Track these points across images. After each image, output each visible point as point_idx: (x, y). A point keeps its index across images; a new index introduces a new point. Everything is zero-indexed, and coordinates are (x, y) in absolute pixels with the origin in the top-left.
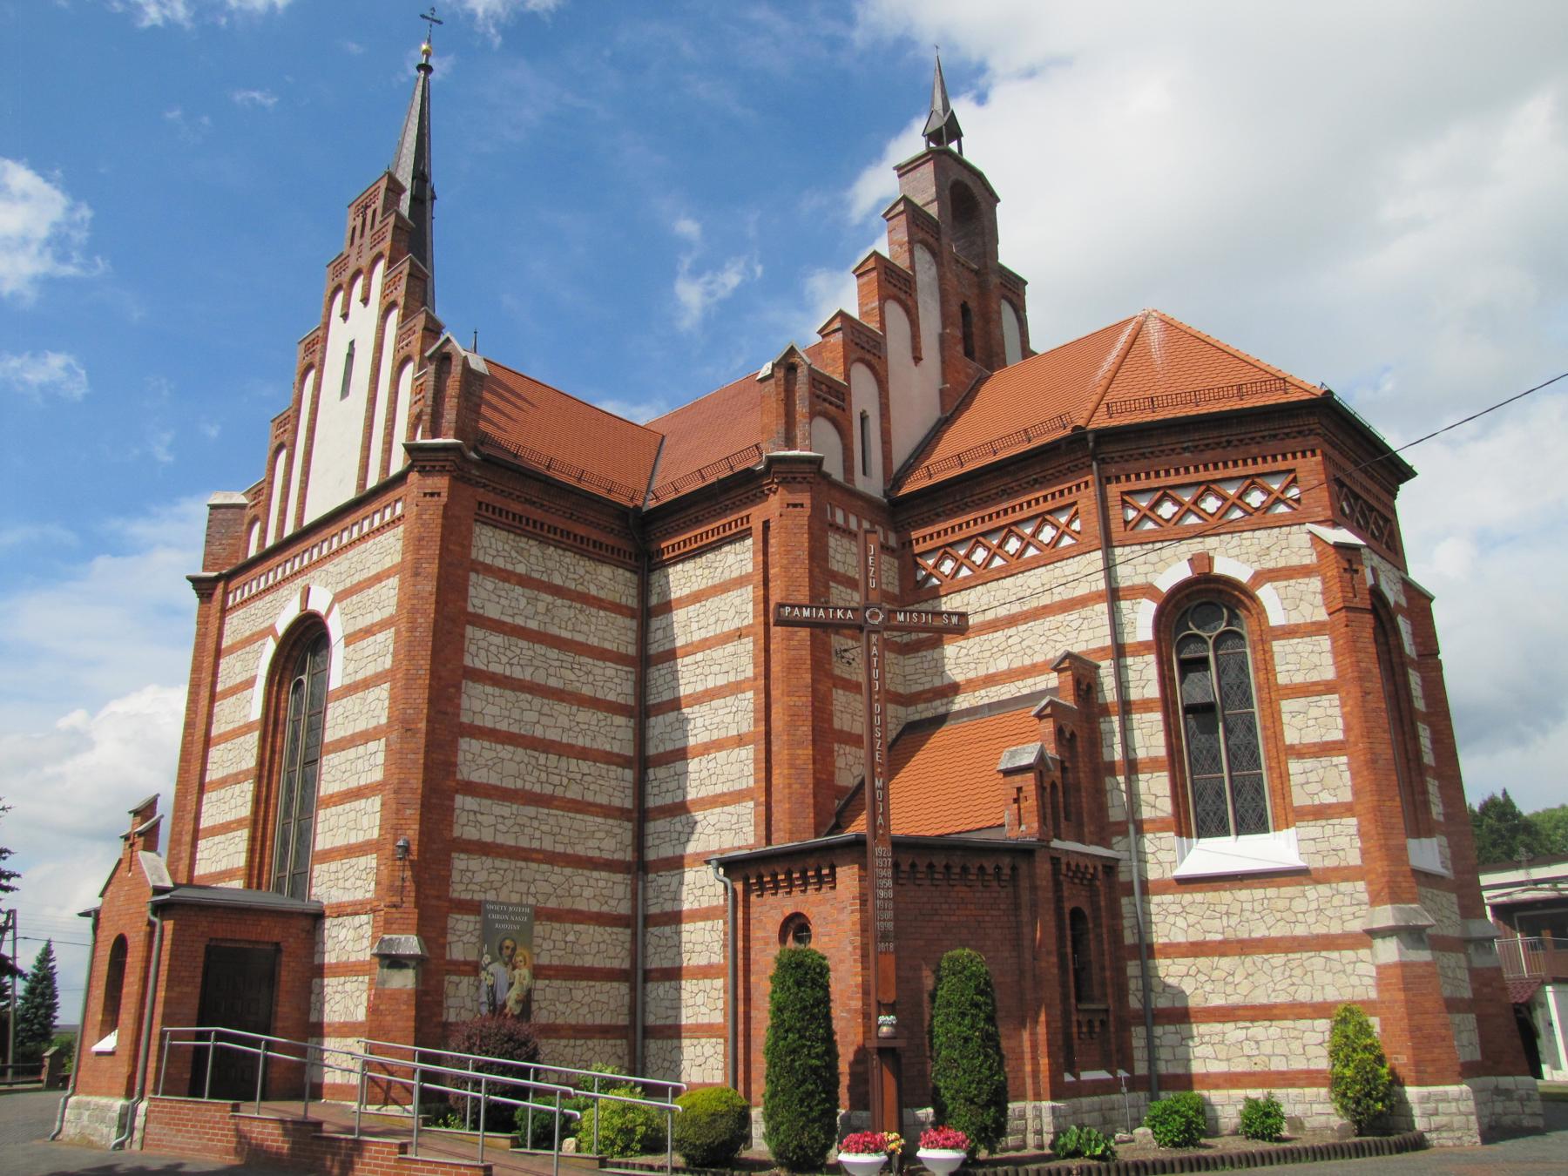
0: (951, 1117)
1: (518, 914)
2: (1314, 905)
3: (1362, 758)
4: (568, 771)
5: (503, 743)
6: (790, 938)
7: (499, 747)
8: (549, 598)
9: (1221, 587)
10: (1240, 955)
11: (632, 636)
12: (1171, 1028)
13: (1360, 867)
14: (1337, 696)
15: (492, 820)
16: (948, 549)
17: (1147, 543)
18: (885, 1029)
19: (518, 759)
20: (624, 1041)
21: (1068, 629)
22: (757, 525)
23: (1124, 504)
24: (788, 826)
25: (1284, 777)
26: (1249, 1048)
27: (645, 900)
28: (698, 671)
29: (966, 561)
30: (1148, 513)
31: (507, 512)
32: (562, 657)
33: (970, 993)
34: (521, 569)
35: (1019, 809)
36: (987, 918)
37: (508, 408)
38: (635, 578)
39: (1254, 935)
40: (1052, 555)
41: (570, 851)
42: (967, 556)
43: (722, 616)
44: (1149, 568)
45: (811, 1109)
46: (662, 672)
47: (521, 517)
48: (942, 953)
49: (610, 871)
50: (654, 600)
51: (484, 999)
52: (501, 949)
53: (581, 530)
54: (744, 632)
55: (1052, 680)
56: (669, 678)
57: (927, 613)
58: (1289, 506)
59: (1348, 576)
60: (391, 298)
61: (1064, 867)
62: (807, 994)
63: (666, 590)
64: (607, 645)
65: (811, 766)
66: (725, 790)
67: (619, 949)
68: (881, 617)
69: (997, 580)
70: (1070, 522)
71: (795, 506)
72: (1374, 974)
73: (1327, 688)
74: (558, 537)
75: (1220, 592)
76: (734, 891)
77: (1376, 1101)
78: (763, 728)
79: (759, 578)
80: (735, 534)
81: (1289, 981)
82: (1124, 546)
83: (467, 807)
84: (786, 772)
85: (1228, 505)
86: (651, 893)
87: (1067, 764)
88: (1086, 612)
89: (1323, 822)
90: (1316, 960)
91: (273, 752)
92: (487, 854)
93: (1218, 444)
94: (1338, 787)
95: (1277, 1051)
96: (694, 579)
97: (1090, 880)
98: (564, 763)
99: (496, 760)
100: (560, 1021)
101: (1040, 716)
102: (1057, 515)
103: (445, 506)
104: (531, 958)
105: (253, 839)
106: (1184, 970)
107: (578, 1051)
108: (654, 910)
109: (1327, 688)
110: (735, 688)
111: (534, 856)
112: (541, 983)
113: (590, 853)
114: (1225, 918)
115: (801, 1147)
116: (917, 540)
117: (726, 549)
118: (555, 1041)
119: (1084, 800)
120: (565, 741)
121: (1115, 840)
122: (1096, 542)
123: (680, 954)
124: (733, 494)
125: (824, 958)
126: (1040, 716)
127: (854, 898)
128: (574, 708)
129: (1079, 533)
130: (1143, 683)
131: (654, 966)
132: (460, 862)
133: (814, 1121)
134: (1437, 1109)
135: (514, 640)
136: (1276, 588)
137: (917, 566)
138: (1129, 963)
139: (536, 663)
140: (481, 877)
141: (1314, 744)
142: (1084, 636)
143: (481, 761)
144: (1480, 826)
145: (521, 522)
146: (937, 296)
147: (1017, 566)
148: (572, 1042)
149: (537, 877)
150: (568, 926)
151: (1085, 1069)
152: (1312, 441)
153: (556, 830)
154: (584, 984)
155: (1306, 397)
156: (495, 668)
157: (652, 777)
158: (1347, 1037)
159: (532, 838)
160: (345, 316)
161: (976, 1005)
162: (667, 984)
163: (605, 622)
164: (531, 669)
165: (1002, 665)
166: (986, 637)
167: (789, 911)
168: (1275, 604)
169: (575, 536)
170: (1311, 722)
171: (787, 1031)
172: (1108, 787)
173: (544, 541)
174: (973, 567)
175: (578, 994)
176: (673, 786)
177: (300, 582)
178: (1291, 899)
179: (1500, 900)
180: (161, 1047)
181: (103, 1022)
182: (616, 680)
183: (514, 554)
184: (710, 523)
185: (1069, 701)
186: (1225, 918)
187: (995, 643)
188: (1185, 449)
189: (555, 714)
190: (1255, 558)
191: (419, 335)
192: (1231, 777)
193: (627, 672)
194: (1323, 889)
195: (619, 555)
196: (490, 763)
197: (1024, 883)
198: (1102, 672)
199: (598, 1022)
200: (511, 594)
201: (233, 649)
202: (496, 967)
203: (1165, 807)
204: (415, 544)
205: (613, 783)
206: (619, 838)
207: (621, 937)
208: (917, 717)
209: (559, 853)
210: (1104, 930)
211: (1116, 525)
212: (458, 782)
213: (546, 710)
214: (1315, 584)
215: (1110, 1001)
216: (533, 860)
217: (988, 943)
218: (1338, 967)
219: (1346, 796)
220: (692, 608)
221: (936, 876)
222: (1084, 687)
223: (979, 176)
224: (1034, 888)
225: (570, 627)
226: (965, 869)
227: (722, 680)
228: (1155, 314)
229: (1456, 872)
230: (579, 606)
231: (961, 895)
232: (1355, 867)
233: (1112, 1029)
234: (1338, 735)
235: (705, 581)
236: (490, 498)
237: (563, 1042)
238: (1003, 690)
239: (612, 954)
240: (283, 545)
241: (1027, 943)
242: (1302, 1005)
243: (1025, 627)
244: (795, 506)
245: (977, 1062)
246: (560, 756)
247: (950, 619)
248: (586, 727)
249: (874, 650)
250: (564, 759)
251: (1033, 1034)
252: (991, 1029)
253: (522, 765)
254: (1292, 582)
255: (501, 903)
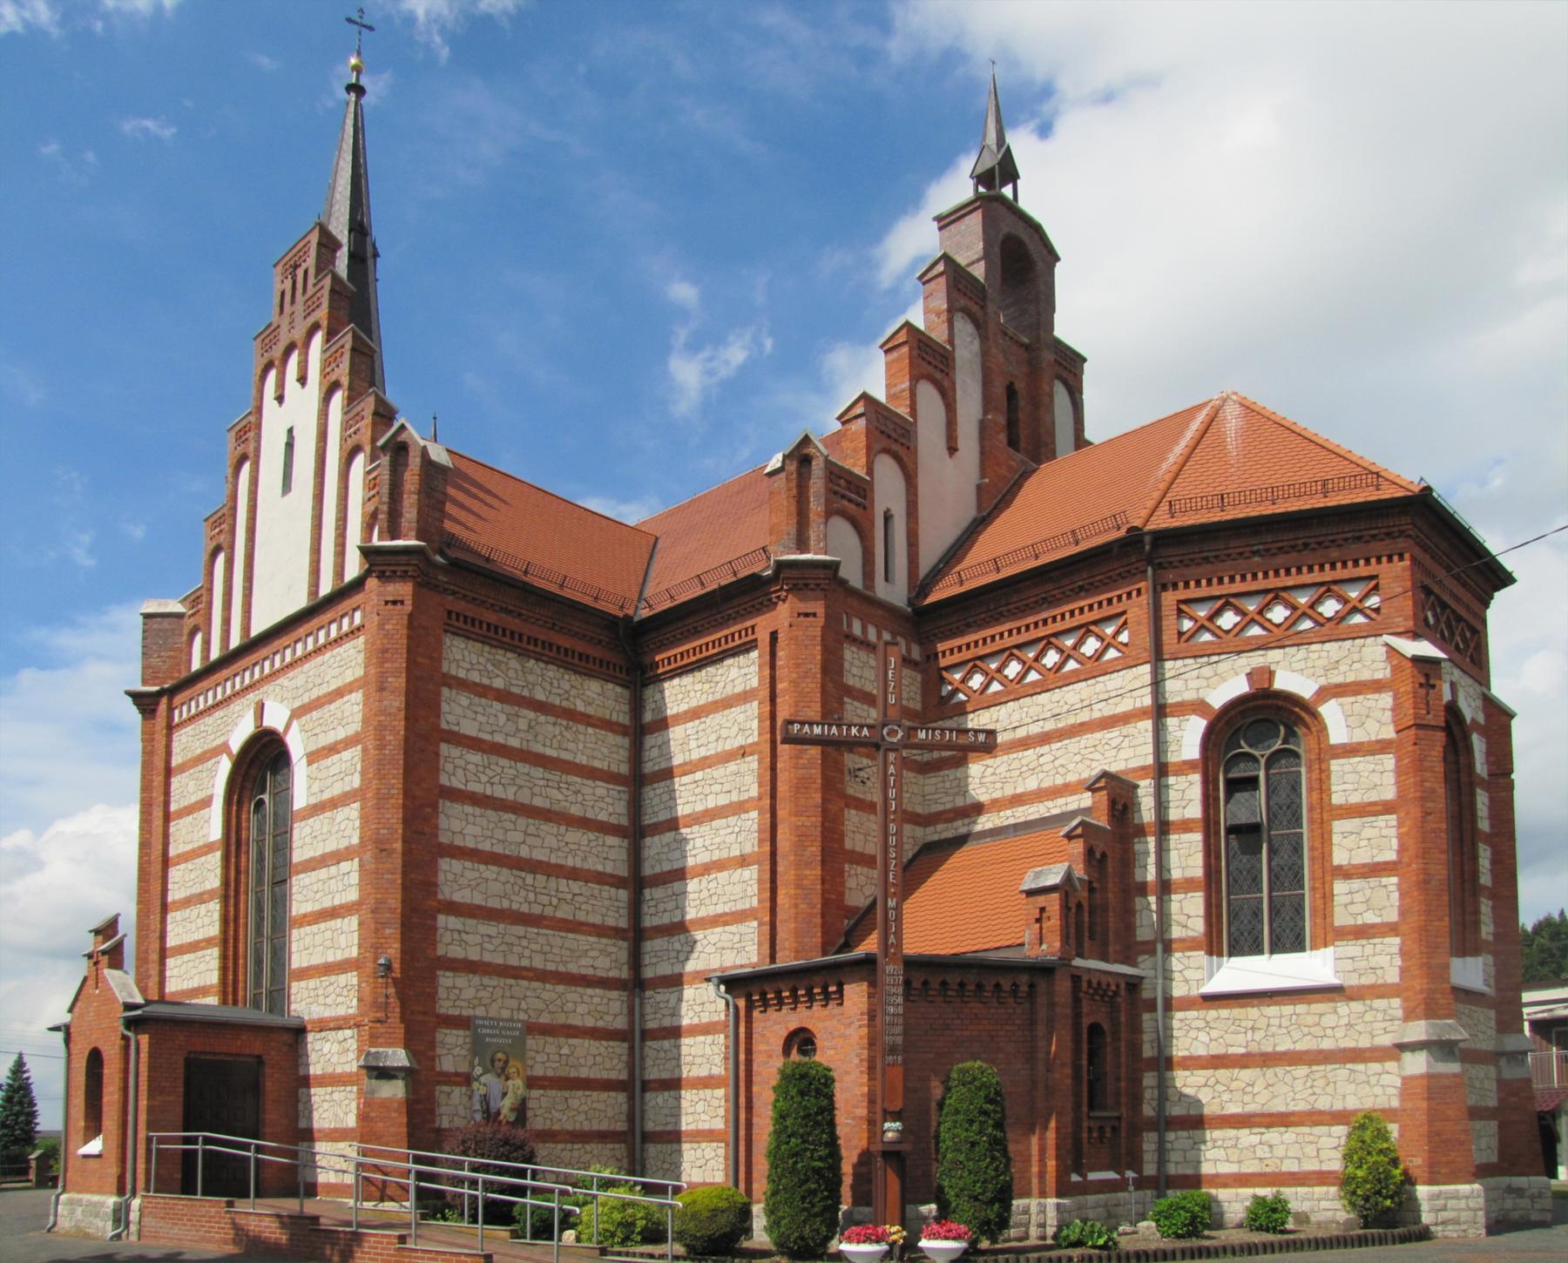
0: (954, 1212)
1: (509, 1029)
2: (1345, 1021)
3: (1414, 878)
4: (557, 891)
5: (486, 863)
6: (795, 1051)
7: (482, 867)
8: (531, 715)
9: (1280, 703)
10: (1262, 1067)
11: (624, 754)
12: (1184, 1134)
13: (1397, 985)
14: (1394, 816)
15: (478, 939)
16: (978, 663)
17: (1202, 656)
18: (890, 1135)
19: (503, 879)
20: (623, 1145)
21: (1107, 747)
22: (763, 636)
23: (1180, 613)
24: (795, 945)
25: (1328, 897)
26: (1262, 1152)
27: (642, 1016)
28: (697, 791)
29: (997, 676)
30: (1207, 624)
31: (481, 622)
32: (547, 775)
33: (980, 1101)
34: (498, 683)
35: (1041, 928)
36: (1000, 1033)
37: (475, 506)
38: (626, 693)
39: (1279, 1049)
40: (1095, 668)
41: (562, 969)
42: (999, 670)
43: (724, 733)
44: (1203, 683)
45: (813, 1206)
46: (658, 792)
47: (496, 627)
48: (952, 1065)
49: (605, 988)
50: (648, 717)
51: (478, 1107)
52: (493, 1061)
53: (564, 642)
54: (748, 750)
55: (1086, 800)
56: (665, 797)
57: (951, 731)
58: (1367, 616)
59: (1422, 691)
60: (333, 378)
61: (1084, 985)
62: (811, 1102)
63: (661, 706)
64: (597, 764)
65: (819, 887)
66: (727, 910)
67: (615, 1061)
68: (900, 734)
69: (1032, 695)
70: (1117, 633)
71: (807, 615)
72: (1399, 1084)
73: (1386, 808)
74: (539, 649)
75: (1279, 708)
76: (736, 1008)
77: (1386, 1198)
78: (767, 848)
79: (766, 693)
80: (739, 646)
81: (1310, 1091)
82: (1176, 659)
83: (451, 926)
84: (792, 892)
85: (1298, 614)
86: (648, 1009)
87: (1095, 885)
88: (1128, 729)
89: (1364, 942)
90: (1341, 1072)
91: (238, 872)
92: (474, 972)
93: (1293, 547)
94: (1384, 907)
95: (1290, 1154)
96: (692, 694)
97: (1112, 997)
98: (553, 882)
99: (479, 881)
100: (556, 1127)
101: (1069, 836)
102: (1102, 626)
103: (410, 616)
104: (525, 1070)
105: (224, 957)
106: (1202, 1081)
107: (576, 1154)
108: (652, 1025)
109: (1386, 808)
110: (738, 808)
111: (524, 973)
112: (535, 1093)
113: (584, 971)
114: (1250, 1032)
115: (802, 1238)
116: (944, 653)
117: (729, 662)
118: (553, 1146)
119: (1111, 920)
120: (553, 861)
121: (1140, 959)
122: (1145, 655)
123: (679, 1066)
124: (736, 602)
125: (830, 1070)
126: (1069, 836)
127: (862, 1014)
128: (563, 828)
129: (1126, 645)
130: (1184, 803)
131: (652, 1077)
132: (446, 979)
133: (816, 1215)
134: (1445, 1205)
135: (494, 758)
136: (1341, 705)
137: (942, 680)
138: (1146, 1074)
139: (518, 781)
140: (469, 993)
141: (1364, 865)
142: (1123, 754)
143: (462, 881)
144: (1530, 946)
145: (496, 633)
146: (979, 376)
147: (1055, 680)
148: (569, 1146)
149: (528, 994)
150: (562, 1040)
151: (1092, 1170)
152: (1401, 543)
153: (547, 949)
154: (580, 1093)
155: (1401, 494)
156: (474, 787)
157: (648, 897)
158: (1363, 1142)
159: (521, 956)
160: (280, 399)
161: (985, 1113)
162: (666, 1094)
163: (593, 739)
164: (515, 788)
165: (1032, 784)
166: (1015, 755)
167: (793, 1026)
168: (1337, 720)
169: (558, 648)
170: (1363, 843)
171: (789, 1136)
172: (1138, 907)
173: (524, 654)
174: (1005, 681)
175: (574, 1103)
176: (671, 905)
177: (252, 697)
178: (1321, 1015)
179: (1540, 1016)
180: (149, 1151)
181: (87, 1128)
182: (607, 800)
183: (490, 667)
184: (711, 634)
185: (1102, 821)
186: (1250, 1032)
187: (1024, 762)
188: (1254, 553)
189: (541, 834)
190: (1322, 672)
191: (368, 420)
192: (1270, 897)
193: (619, 792)
194: (1357, 1006)
195: (608, 668)
196: (473, 883)
197: (1042, 1000)
198: (1140, 792)
199: (595, 1127)
200: (489, 710)
201: (183, 768)
202: (489, 1078)
203: (1198, 926)
204: (379, 656)
205: (607, 903)
206: (614, 958)
207: (618, 1051)
208: (936, 837)
209: (551, 972)
210: (1123, 1044)
211: (1168, 637)
212: (439, 902)
213: (531, 829)
214: (1386, 699)
215: (1123, 1110)
216: (523, 978)
217: (1000, 1056)
218: (1363, 1077)
219: (1392, 916)
220: (690, 724)
221: (950, 993)
222: (1119, 807)
223: (1036, 229)
224: (1052, 1005)
225: (555, 745)
226: (979, 987)
227: (723, 800)
228: (1234, 397)
229: (1498, 989)
230: (564, 723)
231: (975, 1011)
232: (1393, 985)
233: (1123, 1134)
234: (1391, 856)
235: (705, 696)
236: (460, 605)
237: (560, 1146)
238: (1030, 811)
239: (608, 1065)
240: (230, 658)
241: (1041, 1055)
242: (1321, 1113)
243: (1059, 744)
244: (807, 615)
245: (983, 1164)
246: (548, 876)
247: (976, 737)
248: (576, 847)
249: (892, 769)
250: (553, 879)
251: (1042, 1138)
252: (999, 1134)
253: (508, 886)
254: (1360, 698)
255: (491, 1019)
